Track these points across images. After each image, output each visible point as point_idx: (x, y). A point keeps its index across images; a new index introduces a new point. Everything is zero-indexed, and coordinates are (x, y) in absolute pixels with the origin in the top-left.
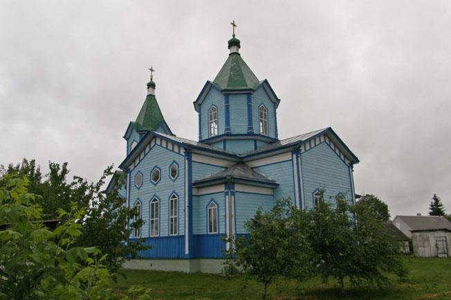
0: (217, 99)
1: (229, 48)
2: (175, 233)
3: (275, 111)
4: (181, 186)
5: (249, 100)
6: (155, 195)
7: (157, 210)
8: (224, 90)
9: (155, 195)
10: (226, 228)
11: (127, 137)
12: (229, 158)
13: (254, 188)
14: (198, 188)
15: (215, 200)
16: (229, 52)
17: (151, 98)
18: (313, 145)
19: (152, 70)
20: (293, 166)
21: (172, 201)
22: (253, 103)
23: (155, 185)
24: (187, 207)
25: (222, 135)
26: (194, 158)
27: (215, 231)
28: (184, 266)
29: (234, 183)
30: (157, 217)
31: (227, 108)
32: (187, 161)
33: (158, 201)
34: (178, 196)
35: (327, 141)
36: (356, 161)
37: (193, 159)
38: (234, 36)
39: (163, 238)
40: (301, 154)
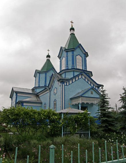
0: (65, 54)
1: (47, 58)
5: (46, 75)
10: (65, 93)
11: (60, 56)
13: (26, 103)
16: (46, 59)
17: (73, 35)
19: (72, 22)
22: (47, 76)
29: (23, 103)
36: (92, 76)
38: (48, 54)
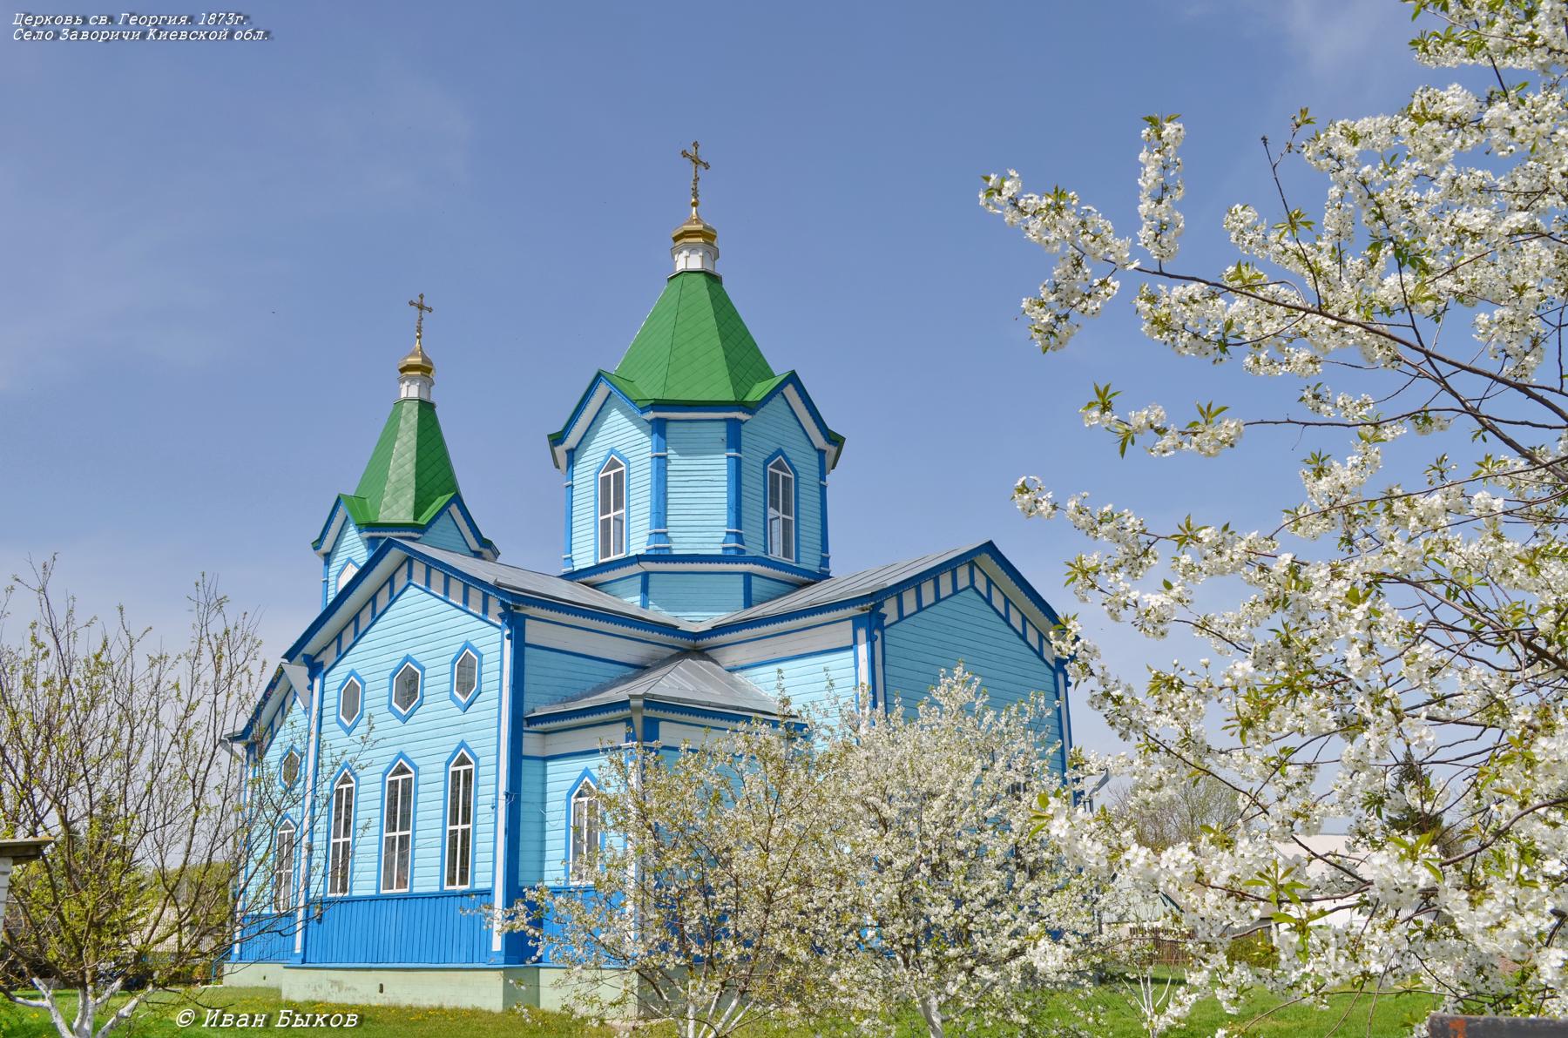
2: (344, 889)
3: (823, 478)
4: (486, 726)
6: (401, 755)
7: (348, 807)
8: (658, 405)
9: (401, 755)
11: (326, 547)
12: (655, 636)
14: (545, 733)
15: (409, 755)
18: (910, 604)
20: (856, 666)
21: (456, 774)
23: (405, 719)
24: (502, 797)
25: (639, 559)
26: (533, 632)
27: (463, 881)
28: (483, 991)
30: (336, 845)
31: (661, 462)
32: (508, 643)
33: (472, 766)
34: (416, 768)
35: (981, 584)
37: (530, 637)
39: (423, 897)
40: (882, 628)
